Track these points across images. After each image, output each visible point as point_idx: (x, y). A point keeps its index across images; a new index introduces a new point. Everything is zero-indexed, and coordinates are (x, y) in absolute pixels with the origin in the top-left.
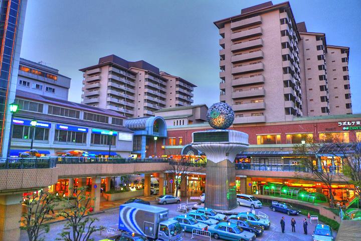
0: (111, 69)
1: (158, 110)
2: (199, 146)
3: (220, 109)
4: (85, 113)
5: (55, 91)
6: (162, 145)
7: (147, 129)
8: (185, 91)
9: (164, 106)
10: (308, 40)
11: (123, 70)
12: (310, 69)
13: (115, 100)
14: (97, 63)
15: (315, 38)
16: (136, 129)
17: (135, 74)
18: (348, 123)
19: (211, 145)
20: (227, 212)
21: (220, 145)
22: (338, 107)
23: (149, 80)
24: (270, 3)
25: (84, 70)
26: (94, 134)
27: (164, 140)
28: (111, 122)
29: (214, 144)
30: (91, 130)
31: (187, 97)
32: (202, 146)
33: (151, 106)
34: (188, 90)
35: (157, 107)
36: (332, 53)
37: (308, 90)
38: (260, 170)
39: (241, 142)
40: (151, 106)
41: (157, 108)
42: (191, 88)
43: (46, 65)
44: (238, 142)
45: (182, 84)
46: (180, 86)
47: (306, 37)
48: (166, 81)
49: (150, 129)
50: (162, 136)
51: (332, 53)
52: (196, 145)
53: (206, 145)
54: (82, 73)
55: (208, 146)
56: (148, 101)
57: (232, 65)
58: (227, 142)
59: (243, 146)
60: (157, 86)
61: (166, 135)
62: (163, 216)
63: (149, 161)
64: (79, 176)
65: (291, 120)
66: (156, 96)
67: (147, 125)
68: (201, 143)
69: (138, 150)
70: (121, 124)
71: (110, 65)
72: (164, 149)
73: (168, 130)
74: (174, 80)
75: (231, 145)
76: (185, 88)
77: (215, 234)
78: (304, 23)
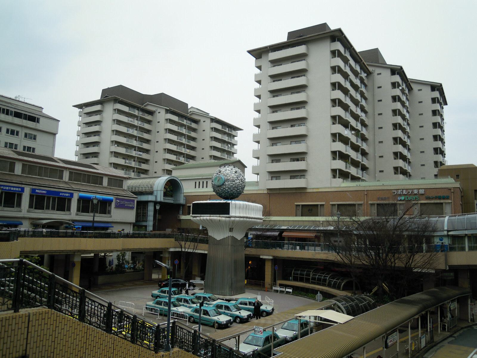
2: (197, 220)
5: (37, 138)
7: (155, 193)
9: (193, 158)
10: (380, 74)
14: (98, 97)
17: (151, 113)
18: (404, 191)
19: (211, 218)
20: (228, 297)
21: (220, 218)
22: (424, 165)
24: (324, 25)
25: (80, 106)
28: (106, 185)
29: (214, 218)
32: (200, 219)
33: (173, 157)
34: (230, 135)
35: (182, 159)
36: (419, 90)
37: (377, 143)
38: (315, 250)
40: (173, 157)
41: (183, 161)
42: (233, 133)
43: (26, 101)
44: (245, 215)
45: (219, 127)
47: (378, 71)
48: (196, 122)
49: (159, 193)
51: (419, 90)
52: (195, 218)
53: (205, 218)
54: (77, 110)
55: (207, 219)
57: (269, 110)
58: (228, 216)
59: (253, 220)
61: (182, 201)
63: (154, 236)
64: (47, 252)
67: (155, 188)
68: (199, 215)
69: (143, 221)
71: (116, 101)
73: (185, 194)
74: (208, 121)
76: (224, 133)
77: (192, 317)
78: (377, 50)
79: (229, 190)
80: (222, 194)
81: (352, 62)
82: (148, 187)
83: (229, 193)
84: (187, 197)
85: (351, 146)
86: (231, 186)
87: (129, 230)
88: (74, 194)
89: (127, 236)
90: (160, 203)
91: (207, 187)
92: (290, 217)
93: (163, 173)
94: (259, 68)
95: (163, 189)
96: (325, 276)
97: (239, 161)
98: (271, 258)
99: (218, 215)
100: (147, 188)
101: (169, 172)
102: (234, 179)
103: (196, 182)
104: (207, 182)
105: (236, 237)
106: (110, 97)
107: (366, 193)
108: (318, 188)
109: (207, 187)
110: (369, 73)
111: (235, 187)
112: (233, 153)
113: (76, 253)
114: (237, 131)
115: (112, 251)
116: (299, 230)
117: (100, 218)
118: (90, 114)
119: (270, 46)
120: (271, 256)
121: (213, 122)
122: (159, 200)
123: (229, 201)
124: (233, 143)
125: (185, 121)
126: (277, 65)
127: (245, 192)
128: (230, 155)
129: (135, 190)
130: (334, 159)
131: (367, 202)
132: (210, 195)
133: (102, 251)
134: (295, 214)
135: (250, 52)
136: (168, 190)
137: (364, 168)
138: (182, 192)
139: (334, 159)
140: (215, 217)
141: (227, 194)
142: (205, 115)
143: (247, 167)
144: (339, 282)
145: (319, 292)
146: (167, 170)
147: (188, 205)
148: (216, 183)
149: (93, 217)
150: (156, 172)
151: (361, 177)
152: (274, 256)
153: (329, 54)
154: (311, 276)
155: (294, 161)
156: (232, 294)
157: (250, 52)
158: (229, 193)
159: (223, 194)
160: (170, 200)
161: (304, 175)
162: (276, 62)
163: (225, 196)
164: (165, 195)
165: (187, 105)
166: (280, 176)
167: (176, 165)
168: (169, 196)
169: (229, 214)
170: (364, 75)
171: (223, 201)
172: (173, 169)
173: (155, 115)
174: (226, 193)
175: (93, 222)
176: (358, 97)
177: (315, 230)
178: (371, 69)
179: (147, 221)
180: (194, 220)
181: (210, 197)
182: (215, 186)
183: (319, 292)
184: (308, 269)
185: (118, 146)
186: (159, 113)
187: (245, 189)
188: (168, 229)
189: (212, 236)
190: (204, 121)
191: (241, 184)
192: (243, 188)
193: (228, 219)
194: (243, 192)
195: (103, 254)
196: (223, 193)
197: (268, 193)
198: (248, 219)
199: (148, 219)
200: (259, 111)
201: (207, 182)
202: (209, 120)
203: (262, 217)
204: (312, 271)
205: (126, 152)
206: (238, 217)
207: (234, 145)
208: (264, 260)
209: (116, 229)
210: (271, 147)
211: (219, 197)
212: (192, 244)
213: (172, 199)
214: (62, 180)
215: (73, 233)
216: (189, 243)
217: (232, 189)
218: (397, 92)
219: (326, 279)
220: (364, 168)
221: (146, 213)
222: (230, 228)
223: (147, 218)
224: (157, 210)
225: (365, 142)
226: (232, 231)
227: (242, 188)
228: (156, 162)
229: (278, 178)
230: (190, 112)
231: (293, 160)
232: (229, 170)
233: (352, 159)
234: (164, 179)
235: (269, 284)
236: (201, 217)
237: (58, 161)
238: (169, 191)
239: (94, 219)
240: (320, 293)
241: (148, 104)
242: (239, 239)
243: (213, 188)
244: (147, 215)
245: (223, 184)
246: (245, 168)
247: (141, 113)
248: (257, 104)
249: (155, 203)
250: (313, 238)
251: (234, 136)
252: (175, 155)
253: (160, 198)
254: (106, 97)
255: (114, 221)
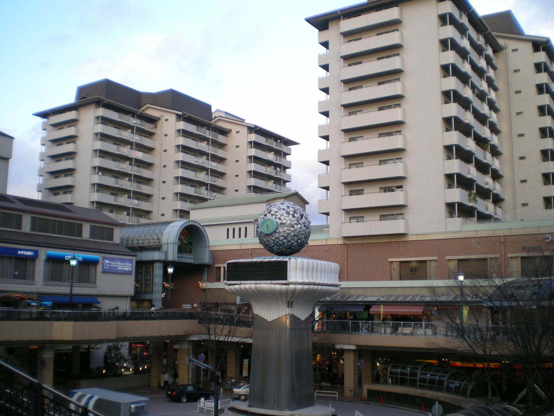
0: (101, 112)
1: (205, 200)
2: (236, 289)
3: (279, 216)
4: (34, 219)
6: (202, 280)
7: (164, 248)
8: (270, 156)
9: (220, 190)
11: (126, 112)
12: (522, 112)
13: (110, 181)
14: (70, 99)
15: (529, 46)
16: (142, 249)
17: (153, 121)
21: (273, 286)
23: (186, 133)
25: (44, 115)
26: (50, 259)
27: (206, 270)
29: (262, 285)
30: (44, 253)
31: (275, 169)
33: (190, 190)
34: (278, 153)
39: (312, 281)
40: (190, 190)
42: (284, 148)
44: (306, 281)
45: (262, 140)
46: (257, 145)
47: (511, 45)
48: (224, 132)
50: (201, 262)
52: (231, 287)
53: (247, 286)
54: (40, 120)
56: (184, 181)
58: (284, 282)
59: (324, 287)
60: (203, 146)
61: (206, 260)
62: (136, 408)
65: (458, 229)
66: (202, 169)
67: (164, 240)
69: (146, 292)
70: (111, 238)
71: (99, 103)
72: (205, 290)
73: (211, 249)
75: (292, 287)
76: (269, 149)
79: (285, 241)
80: (274, 246)
81: (472, 32)
82: (153, 239)
83: (285, 245)
84: (214, 254)
85: (476, 166)
86: (289, 234)
87: (125, 306)
88: (39, 251)
89: (124, 317)
90: (173, 264)
91: (246, 236)
92: (382, 282)
93: (175, 216)
94: (325, 45)
95: (177, 241)
96: (440, 376)
97: (296, 194)
98: (353, 347)
99: (269, 282)
100: (152, 241)
101: (184, 214)
102: (293, 223)
103: (228, 229)
104: (246, 228)
105: (298, 316)
106: (90, 98)
107: (503, 240)
108: (425, 234)
109: (246, 236)
110: (497, 49)
111: (294, 235)
112: (285, 182)
113: (46, 345)
114: (290, 147)
115: (101, 341)
116: (397, 302)
117: (80, 290)
118: (58, 126)
119: (342, 11)
120: (354, 345)
121: (251, 133)
122: (171, 258)
123: (286, 259)
124: (285, 165)
125: (208, 131)
126: (354, 40)
127: (310, 243)
128: (280, 185)
129: (133, 244)
130: (450, 186)
131: (505, 255)
132: (251, 249)
133: (85, 342)
134: (389, 277)
135: (310, 21)
136: (185, 242)
137: (497, 200)
138: (207, 246)
139: (450, 186)
140: (265, 285)
141: (281, 246)
142: (239, 121)
143: (308, 203)
144: (465, 385)
145: (437, 402)
146: (181, 211)
147: (216, 266)
148: (264, 230)
149: (69, 288)
150: (163, 215)
151: (493, 214)
152: (357, 346)
153: (435, 21)
154: (419, 375)
155: (385, 191)
156: (294, 407)
157: (310, 21)
158: (285, 245)
159: (275, 248)
160: (188, 259)
161: (402, 214)
162: (349, 35)
163: (279, 251)
164: (181, 250)
165: (209, 107)
166: (363, 217)
167: (195, 203)
168: (186, 252)
169: (286, 279)
170: (489, 51)
171: (275, 258)
172: (191, 209)
173: (159, 124)
174: (280, 245)
175: (71, 295)
176: (484, 86)
177: (422, 302)
178: (501, 42)
179: (152, 293)
180: (230, 289)
181: (253, 252)
182: (262, 235)
183: (437, 402)
184: (414, 365)
185: (103, 174)
186: (167, 120)
187: (312, 237)
188: (185, 305)
189: (260, 315)
190: (238, 132)
191: (303, 231)
192: (307, 237)
193: (284, 287)
194: (307, 244)
195: (86, 346)
196: (276, 245)
197: (344, 244)
198: (316, 287)
199: (154, 290)
200: (326, 114)
201: (246, 228)
202: (246, 129)
203: (337, 282)
204: (420, 367)
205: (116, 184)
206: (299, 284)
207: (285, 168)
208: (342, 352)
209: (106, 306)
210: (348, 169)
211: (270, 253)
212: (227, 327)
213: (191, 257)
214: (20, 231)
215: (41, 313)
216: (221, 326)
217: (289, 238)
218: (544, 78)
219: (444, 381)
220: (497, 200)
221: (150, 279)
222: (289, 302)
223: (152, 287)
224: (169, 274)
225: (498, 159)
226: (291, 307)
227: (305, 238)
228: (163, 198)
229: (359, 219)
230: (215, 117)
231: (386, 190)
232: (284, 209)
233: (478, 186)
234: (178, 225)
235: (351, 391)
236: (241, 284)
237: (15, 201)
238: (186, 245)
239: (71, 290)
240: (439, 403)
241: (148, 107)
242: (303, 319)
243: (260, 238)
244: (152, 283)
245: (275, 232)
246: (307, 205)
247: (139, 122)
248: (324, 102)
249: (166, 264)
250: (420, 315)
251: (285, 154)
252: (192, 186)
253: (172, 255)
254: (84, 98)
255: (100, 293)
